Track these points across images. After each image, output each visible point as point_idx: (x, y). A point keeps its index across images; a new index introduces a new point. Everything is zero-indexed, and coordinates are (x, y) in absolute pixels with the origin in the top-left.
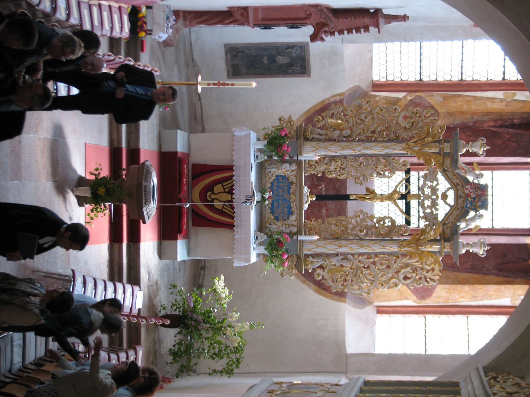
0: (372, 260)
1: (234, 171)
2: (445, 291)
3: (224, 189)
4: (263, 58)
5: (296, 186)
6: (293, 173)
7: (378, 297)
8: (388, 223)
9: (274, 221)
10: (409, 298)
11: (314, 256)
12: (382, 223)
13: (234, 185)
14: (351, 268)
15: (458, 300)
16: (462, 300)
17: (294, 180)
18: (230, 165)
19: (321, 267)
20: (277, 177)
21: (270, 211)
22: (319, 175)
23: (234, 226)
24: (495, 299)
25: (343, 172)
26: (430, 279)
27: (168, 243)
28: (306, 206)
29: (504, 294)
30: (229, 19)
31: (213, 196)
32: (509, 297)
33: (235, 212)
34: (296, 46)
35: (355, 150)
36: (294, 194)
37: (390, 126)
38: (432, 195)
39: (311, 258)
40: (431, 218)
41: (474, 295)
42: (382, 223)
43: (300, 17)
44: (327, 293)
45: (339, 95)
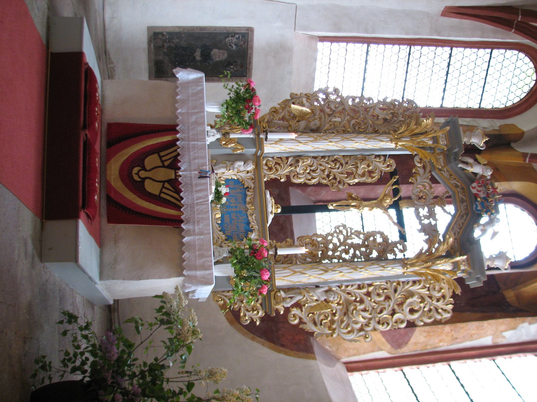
0: (364, 290)
1: (177, 132)
2: (425, 334)
3: (163, 162)
4: (195, 51)
6: (249, 174)
7: (346, 350)
8: (379, 240)
9: (226, 242)
10: (383, 347)
11: (287, 289)
12: (372, 239)
13: (179, 154)
14: (338, 304)
15: (438, 345)
16: (441, 344)
18: (172, 123)
19: (298, 305)
21: (219, 229)
22: (282, 180)
23: (182, 221)
24: (476, 339)
25: (314, 175)
26: (442, 309)
27: (56, 227)
28: (271, 217)
29: (486, 332)
31: (143, 174)
32: (490, 335)
34: (237, 34)
35: (331, 142)
36: (252, 203)
39: (282, 294)
41: (455, 336)
42: (372, 239)
44: (288, 350)
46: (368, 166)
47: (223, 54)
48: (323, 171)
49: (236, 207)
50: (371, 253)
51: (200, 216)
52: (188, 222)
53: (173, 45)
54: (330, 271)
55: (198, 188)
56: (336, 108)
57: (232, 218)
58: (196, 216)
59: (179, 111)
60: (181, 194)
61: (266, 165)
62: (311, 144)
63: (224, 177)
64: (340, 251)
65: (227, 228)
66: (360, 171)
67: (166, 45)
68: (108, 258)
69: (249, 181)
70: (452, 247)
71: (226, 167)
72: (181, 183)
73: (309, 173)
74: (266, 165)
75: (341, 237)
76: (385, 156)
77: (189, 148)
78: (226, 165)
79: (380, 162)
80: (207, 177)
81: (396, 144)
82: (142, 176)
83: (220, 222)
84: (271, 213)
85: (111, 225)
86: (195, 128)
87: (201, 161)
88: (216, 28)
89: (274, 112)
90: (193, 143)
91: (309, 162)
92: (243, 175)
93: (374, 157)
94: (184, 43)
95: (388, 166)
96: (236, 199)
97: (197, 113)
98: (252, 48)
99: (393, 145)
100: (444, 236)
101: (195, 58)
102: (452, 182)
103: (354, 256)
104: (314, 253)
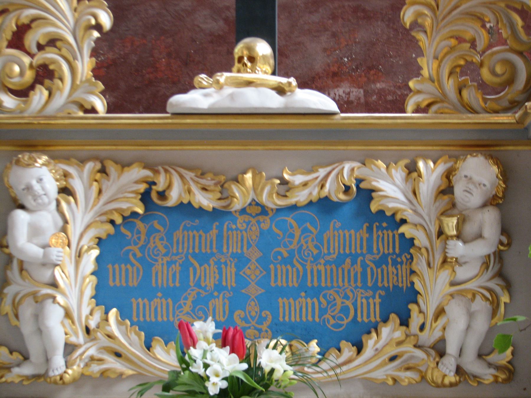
5: (169, 166)
6: (77, 185)
9: (416, 320)
20: (103, 297)
21: (348, 351)
22: (106, 19)
49: (241, 261)
57: (294, 283)
61: (23, 93)
63: (86, 311)
65: (345, 310)
69: (437, 334)
71: (39, 300)
74: (23, 93)
78: (29, 301)
84: (280, 91)
92: (81, 215)
96: (203, 259)
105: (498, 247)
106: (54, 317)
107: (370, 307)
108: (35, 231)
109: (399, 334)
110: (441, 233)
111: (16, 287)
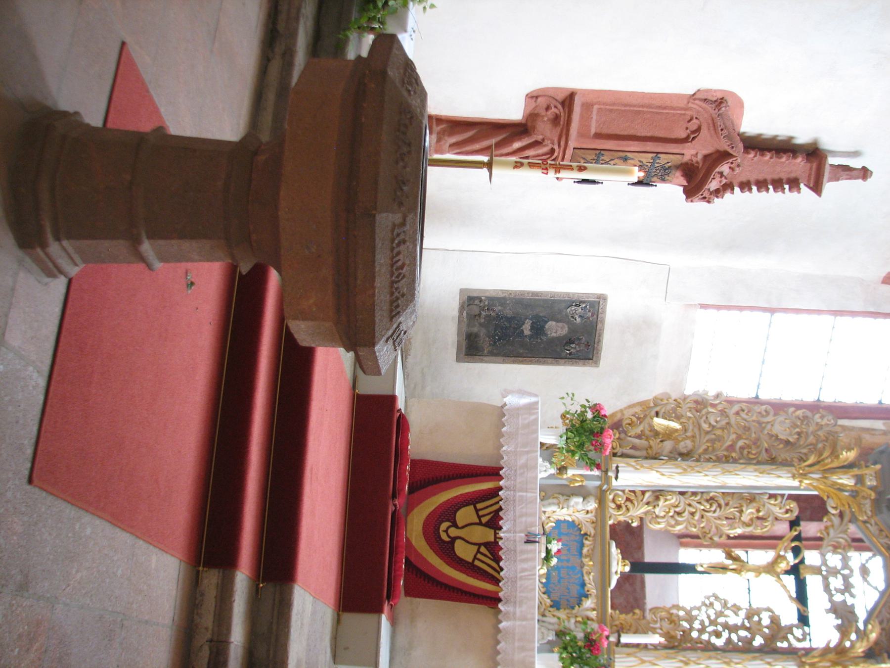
1: (501, 478)
3: (479, 517)
4: (524, 323)
5: (594, 541)
6: (589, 515)
9: (551, 609)
12: (756, 618)
13: (501, 509)
17: (588, 528)
18: (493, 465)
20: (558, 522)
21: (543, 590)
23: (500, 600)
27: (356, 621)
28: (613, 583)
30: (520, 140)
31: (453, 532)
33: (502, 569)
34: (584, 302)
36: (590, 556)
37: (758, 439)
38: (844, 568)
40: (844, 614)
42: (756, 618)
43: (673, 136)
45: (641, 404)
46: (758, 511)
47: (562, 328)
48: (693, 514)
49: (568, 561)
50: (753, 639)
51: (523, 595)
52: (507, 601)
53: (493, 314)
54: (692, 663)
55: (524, 556)
56: (717, 422)
58: (518, 594)
59: (504, 448)
60: (501, 564)
61: (613, 501)
62: (677, 477)
64: (709, 633)
66: (745, 518)
67: (484, 313)
68: (401, 640)
69: (588, 524)
70: (877, 643)
71: (558, 504)
72: (501, 549)
73: (672, 517)
74: (613, 501)
75: (711, 612)
76: (783, 496)
77: (514, 501)
79: (775, 505)
80: (535, 542)
81: (800, 482)
82: (452, 535)
83: (544, 581)
84: (616, 572)
85: (409, 598)
86: (524, 473)
87: (529, 519)
88: (554, 294)
89: (629, 424)
90: (521, 494)
91: (673, 501)
92: (581, 516)
93: (767, 496)
94: (508, 312)
95: (787, 512)
97: (528, 452)
98: (603, 322)
99: (796, 483)
100: (866, 623)
101: (522, 331)
102: (882, 541)
103: (729, 640)
104: (672, 633)
105: (743, 622)
106: (554, 508)
107: (555, 597)
108: (577, 503)
109: (548, 604)
110: (576, 617)
111: (562, 498)
